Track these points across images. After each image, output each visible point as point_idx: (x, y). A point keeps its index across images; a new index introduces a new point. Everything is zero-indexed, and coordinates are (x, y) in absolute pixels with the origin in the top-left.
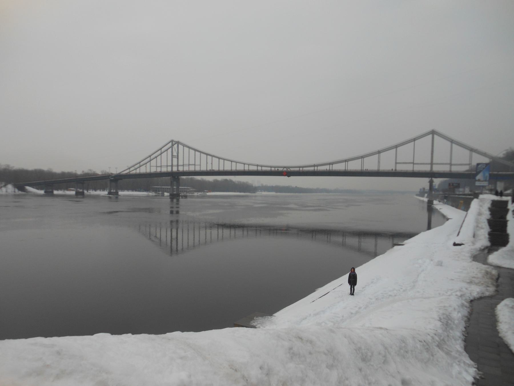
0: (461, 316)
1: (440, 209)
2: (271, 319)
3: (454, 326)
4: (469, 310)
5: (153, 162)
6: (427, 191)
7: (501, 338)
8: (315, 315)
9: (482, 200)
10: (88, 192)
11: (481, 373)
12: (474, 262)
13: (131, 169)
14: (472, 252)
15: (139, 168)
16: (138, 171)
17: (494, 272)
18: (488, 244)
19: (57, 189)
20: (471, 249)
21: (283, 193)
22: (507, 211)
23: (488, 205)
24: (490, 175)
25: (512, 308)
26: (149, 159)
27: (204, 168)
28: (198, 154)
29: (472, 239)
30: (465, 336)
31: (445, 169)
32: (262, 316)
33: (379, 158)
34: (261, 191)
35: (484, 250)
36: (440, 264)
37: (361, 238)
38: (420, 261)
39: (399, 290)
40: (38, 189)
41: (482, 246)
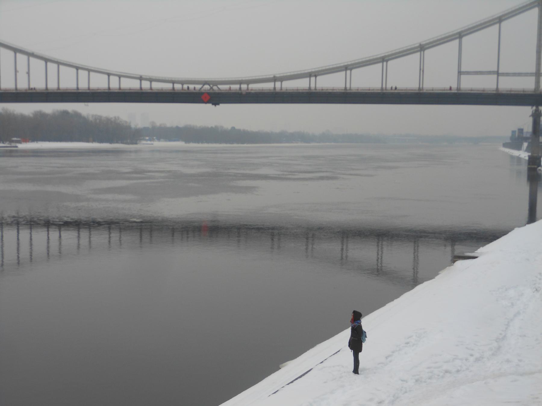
6: (528, 135)
34: (150, 140)
39: (466, 360)
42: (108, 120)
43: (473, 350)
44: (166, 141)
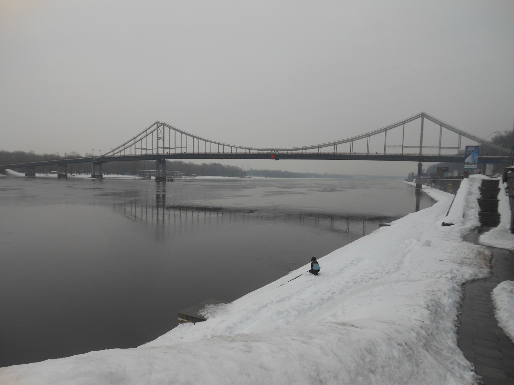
0: (452, 302)
1: (428, 192)
2: (226, 306)
3: (444, 315)
4: (460, 295)
5: (138, 145)
6: (416, 176)
7: (500, 329)
8: (279, 302)
9: (472, 180)
10: (71, 175)
11: (479, 377)
12: (465, 242)
13: (115, 152)
14: (462, 232)
15: (123, 151)
16: (122, 154)
17: (487, 252)
18: (479, 224)
19: (40, 172)
20: (462, 229)
21: (272, 177)
22: (498, 190)
23: (478, 184)
24: (479, 158)
25: (511, 291)
26: (133, 141)
27: (190, 151)
28: (184, 136)
29: (462, 219)
30: (458, 327)
31: (434, 152)
32: (215, 304)
33: (368, 141)
34: (250, 176)
35: (474, 230)
36: (428, 244)
37: (349, 221)
38: (407, 241)
39: (382, 273)
40: (19, 172)
41: (472, 226)
42: (233, 167)
43: (385, 268)
44: (257, 176)
